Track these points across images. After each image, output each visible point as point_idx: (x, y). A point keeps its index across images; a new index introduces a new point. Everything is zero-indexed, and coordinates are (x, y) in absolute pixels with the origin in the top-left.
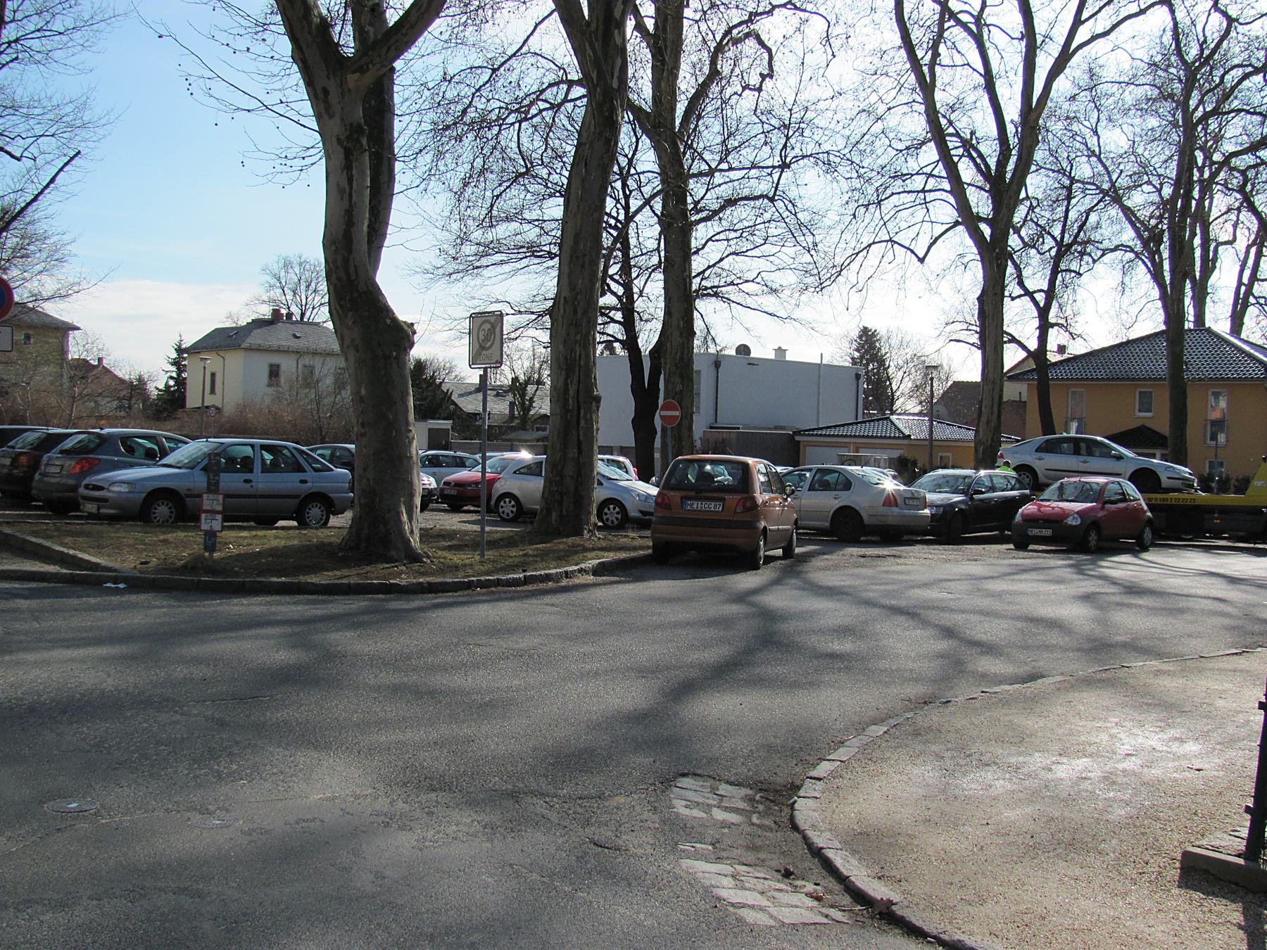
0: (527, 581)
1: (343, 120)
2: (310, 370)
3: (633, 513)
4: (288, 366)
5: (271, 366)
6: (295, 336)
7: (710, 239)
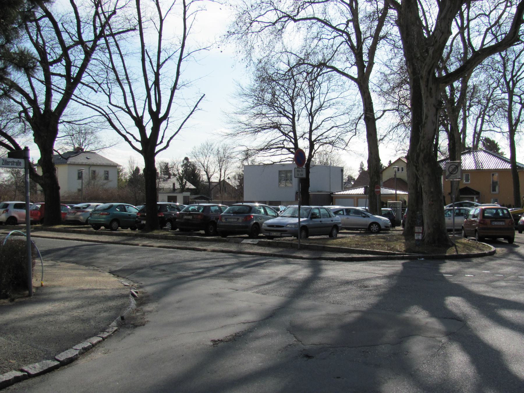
0: (211, 259)
1: (436, 99)
2: (94, 172)
3: (383, 227)
4: (85, 171)
5: (105, 171)
6: (87, 158)
7: (323, 121)
